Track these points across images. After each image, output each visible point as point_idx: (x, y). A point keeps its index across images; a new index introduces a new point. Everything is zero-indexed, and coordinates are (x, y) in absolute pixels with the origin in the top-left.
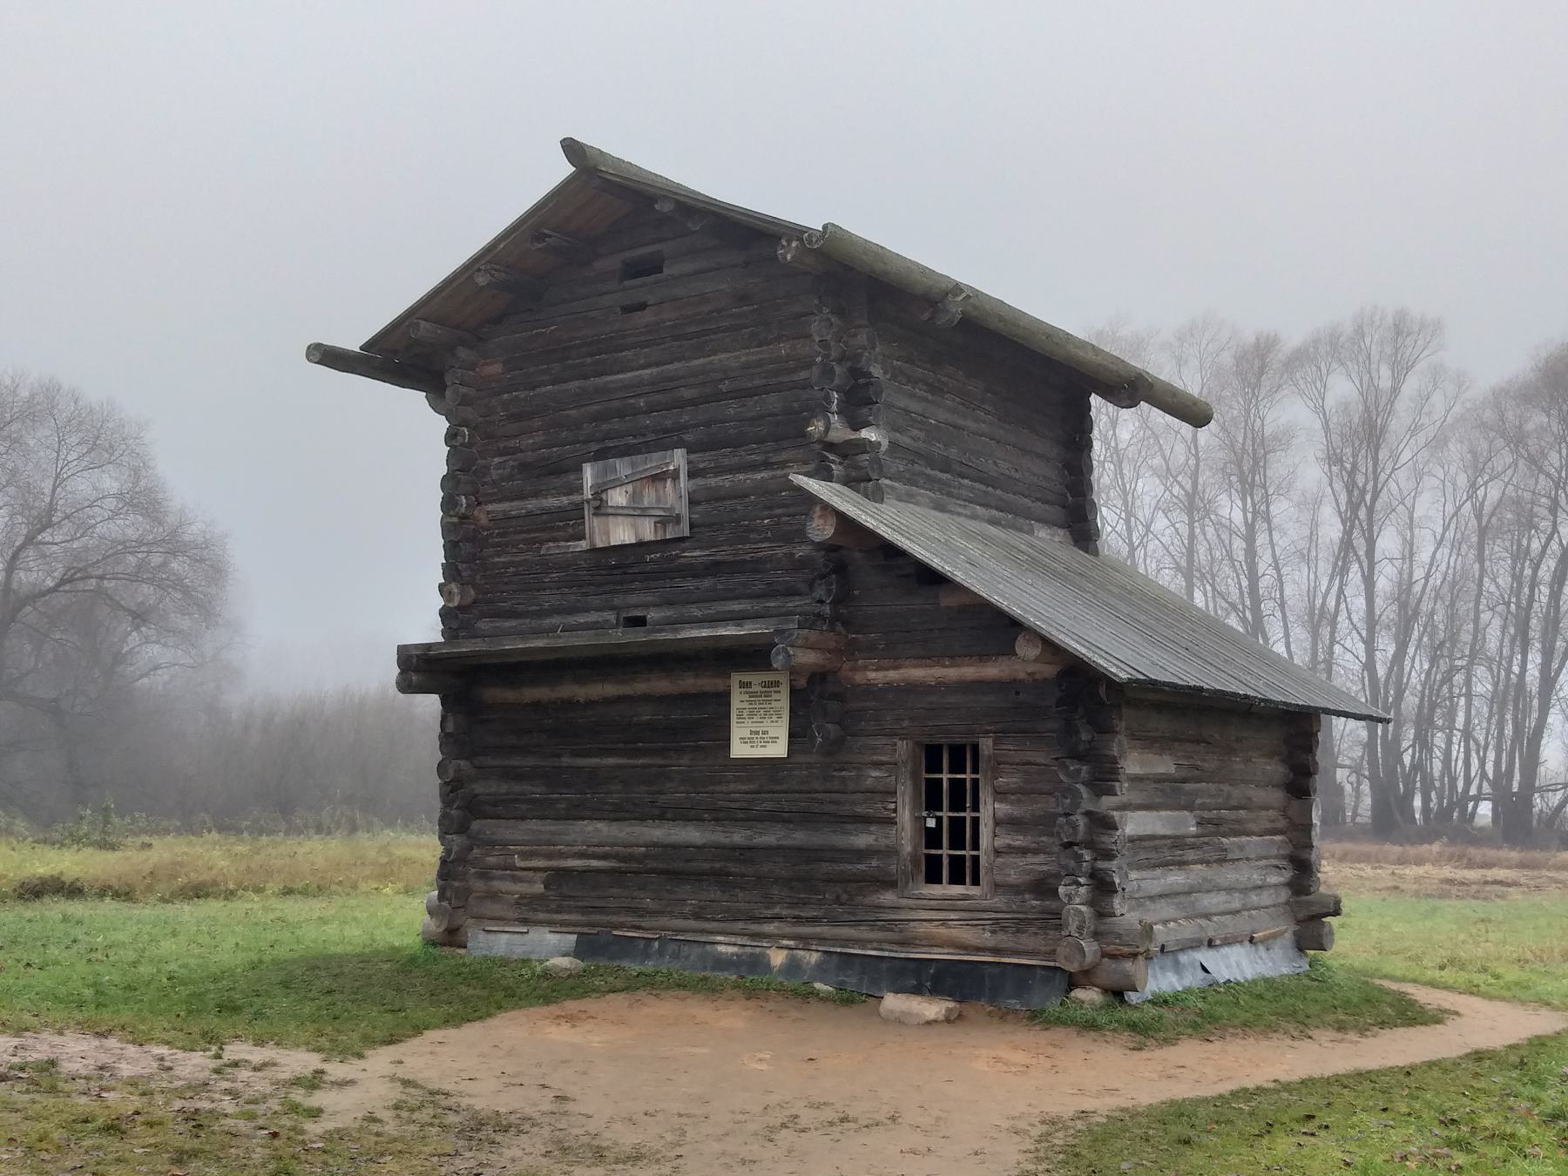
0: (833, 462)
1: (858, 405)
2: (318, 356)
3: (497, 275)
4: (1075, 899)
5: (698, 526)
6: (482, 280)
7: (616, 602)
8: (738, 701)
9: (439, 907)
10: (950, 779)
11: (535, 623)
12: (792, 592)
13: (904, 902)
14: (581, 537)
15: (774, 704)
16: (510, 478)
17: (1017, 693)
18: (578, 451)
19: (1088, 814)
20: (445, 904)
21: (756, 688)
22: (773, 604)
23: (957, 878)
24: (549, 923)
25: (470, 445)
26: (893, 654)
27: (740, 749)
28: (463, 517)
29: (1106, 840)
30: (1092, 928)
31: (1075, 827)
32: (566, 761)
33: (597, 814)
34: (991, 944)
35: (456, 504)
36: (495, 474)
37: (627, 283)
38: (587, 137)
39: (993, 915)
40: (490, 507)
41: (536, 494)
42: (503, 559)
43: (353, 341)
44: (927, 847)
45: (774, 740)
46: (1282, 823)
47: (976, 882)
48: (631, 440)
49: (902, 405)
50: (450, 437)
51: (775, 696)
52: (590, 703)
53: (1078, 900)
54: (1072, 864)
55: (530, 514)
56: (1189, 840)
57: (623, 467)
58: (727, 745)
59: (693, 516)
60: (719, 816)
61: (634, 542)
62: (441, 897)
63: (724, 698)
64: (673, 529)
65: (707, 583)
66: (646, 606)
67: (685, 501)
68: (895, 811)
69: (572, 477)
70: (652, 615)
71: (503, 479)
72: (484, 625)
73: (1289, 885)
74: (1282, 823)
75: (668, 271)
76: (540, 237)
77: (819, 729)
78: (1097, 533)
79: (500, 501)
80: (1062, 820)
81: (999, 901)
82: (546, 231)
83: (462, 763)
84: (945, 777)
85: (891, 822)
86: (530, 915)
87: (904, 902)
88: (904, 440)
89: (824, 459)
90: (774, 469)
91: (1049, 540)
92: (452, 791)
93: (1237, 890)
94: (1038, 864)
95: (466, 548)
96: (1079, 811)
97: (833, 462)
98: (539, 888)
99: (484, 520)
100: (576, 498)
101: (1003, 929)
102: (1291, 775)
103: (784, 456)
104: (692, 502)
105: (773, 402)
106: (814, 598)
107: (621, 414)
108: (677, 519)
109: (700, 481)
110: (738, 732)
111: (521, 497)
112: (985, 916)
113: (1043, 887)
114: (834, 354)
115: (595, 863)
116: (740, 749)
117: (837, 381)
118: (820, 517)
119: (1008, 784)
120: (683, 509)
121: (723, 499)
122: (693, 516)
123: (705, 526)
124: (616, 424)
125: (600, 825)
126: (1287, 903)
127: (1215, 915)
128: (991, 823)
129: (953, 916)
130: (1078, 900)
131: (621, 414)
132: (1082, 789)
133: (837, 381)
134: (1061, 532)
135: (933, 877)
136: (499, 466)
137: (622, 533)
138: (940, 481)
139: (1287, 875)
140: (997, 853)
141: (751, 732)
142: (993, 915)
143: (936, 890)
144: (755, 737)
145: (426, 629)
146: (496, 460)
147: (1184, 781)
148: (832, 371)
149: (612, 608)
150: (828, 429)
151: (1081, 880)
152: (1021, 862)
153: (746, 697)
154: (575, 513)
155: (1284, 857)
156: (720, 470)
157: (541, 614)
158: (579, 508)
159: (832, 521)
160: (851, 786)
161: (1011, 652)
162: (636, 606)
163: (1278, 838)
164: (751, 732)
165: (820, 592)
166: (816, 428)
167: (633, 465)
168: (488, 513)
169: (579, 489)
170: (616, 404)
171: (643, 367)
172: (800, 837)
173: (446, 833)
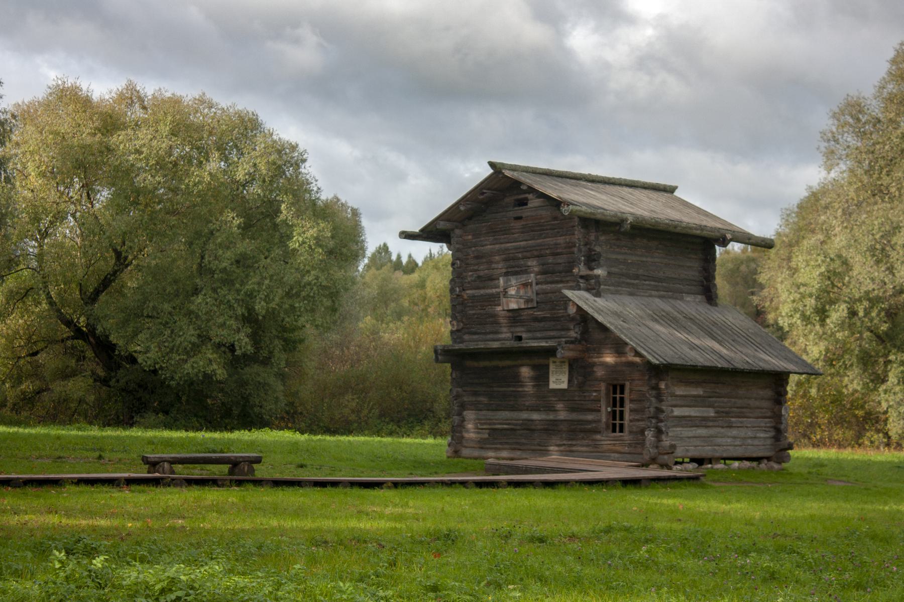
1: (592, 260)
2: (403, 236)
6: (462, 208)
8: (552, 368)
13: (603, 438)
19: (656, 408)
24: (491, 449)
25: (460, 267)
27: (552, 386)
28: (458, 296)
29: (662, 416)
32: (495, 389)
33: (506, 408)
35: (455, 291)
36: (469, 279)
37: (516, 208)
38: (497, 160)
40: (468, 292)
41: (484, 288)
43: (417, 229)
45: (563, 382)
46: (769, 414)
48: (517, 269)
52: (503, 368)
54: (649, 424)
55: (482, 295)
57: (513, 281)
58: (548, 385)
63: (547, 366)
65: (542, 324)
66: (522, 332)
67: (535, 294)
69: (497, 282)
71: (472, 281)
72: (466, 337)
73: (774, 437)
74: (769, 414)
75: (530, 205)
77: (576, 378)
78: (717, 297)
79: (471, 289)
82: (485, 191)
83: (459, 389)
85: (599, 411)
86: (483, 446)
87: (603, 438)
88: (614, 270)
89: (578, 282)
91: (692, 305)
93: (738, 438)
95: (459, 308)
98: (486, 436)
99: (465, 297)
100: (497, 290)
101: (631, 446)
103: (568, 279)
108: (532, 300)
109: (540, 286)
110: (552, 379)
111: (478, 288)
114: (582, 243)
115: (505, 426)
116: (552, 386)
117: (583, 253)
120: (534, 297)
121: (548, 293)
123: (542, 303)
125: (507, 413)
126: (772, 445)
134: (699, 297)
135: (614, 431)
136: (472, 276)
138: (633, 284)
139: (772, 434)
140: (631, 421)
143: (614, 434)
144: (558, 381)
145: (445, 339)
146: (470, 273)
147: (710, 397)
155: (771, 427)
156: (547, 283)
157: (486, 333)
158: (498, 294)
159: (575, 307)
160: (587, 399)
163: (767, 420)
166: (575, 271)
167: (517, 279)
170: (511, 255)
171: (521, 241)
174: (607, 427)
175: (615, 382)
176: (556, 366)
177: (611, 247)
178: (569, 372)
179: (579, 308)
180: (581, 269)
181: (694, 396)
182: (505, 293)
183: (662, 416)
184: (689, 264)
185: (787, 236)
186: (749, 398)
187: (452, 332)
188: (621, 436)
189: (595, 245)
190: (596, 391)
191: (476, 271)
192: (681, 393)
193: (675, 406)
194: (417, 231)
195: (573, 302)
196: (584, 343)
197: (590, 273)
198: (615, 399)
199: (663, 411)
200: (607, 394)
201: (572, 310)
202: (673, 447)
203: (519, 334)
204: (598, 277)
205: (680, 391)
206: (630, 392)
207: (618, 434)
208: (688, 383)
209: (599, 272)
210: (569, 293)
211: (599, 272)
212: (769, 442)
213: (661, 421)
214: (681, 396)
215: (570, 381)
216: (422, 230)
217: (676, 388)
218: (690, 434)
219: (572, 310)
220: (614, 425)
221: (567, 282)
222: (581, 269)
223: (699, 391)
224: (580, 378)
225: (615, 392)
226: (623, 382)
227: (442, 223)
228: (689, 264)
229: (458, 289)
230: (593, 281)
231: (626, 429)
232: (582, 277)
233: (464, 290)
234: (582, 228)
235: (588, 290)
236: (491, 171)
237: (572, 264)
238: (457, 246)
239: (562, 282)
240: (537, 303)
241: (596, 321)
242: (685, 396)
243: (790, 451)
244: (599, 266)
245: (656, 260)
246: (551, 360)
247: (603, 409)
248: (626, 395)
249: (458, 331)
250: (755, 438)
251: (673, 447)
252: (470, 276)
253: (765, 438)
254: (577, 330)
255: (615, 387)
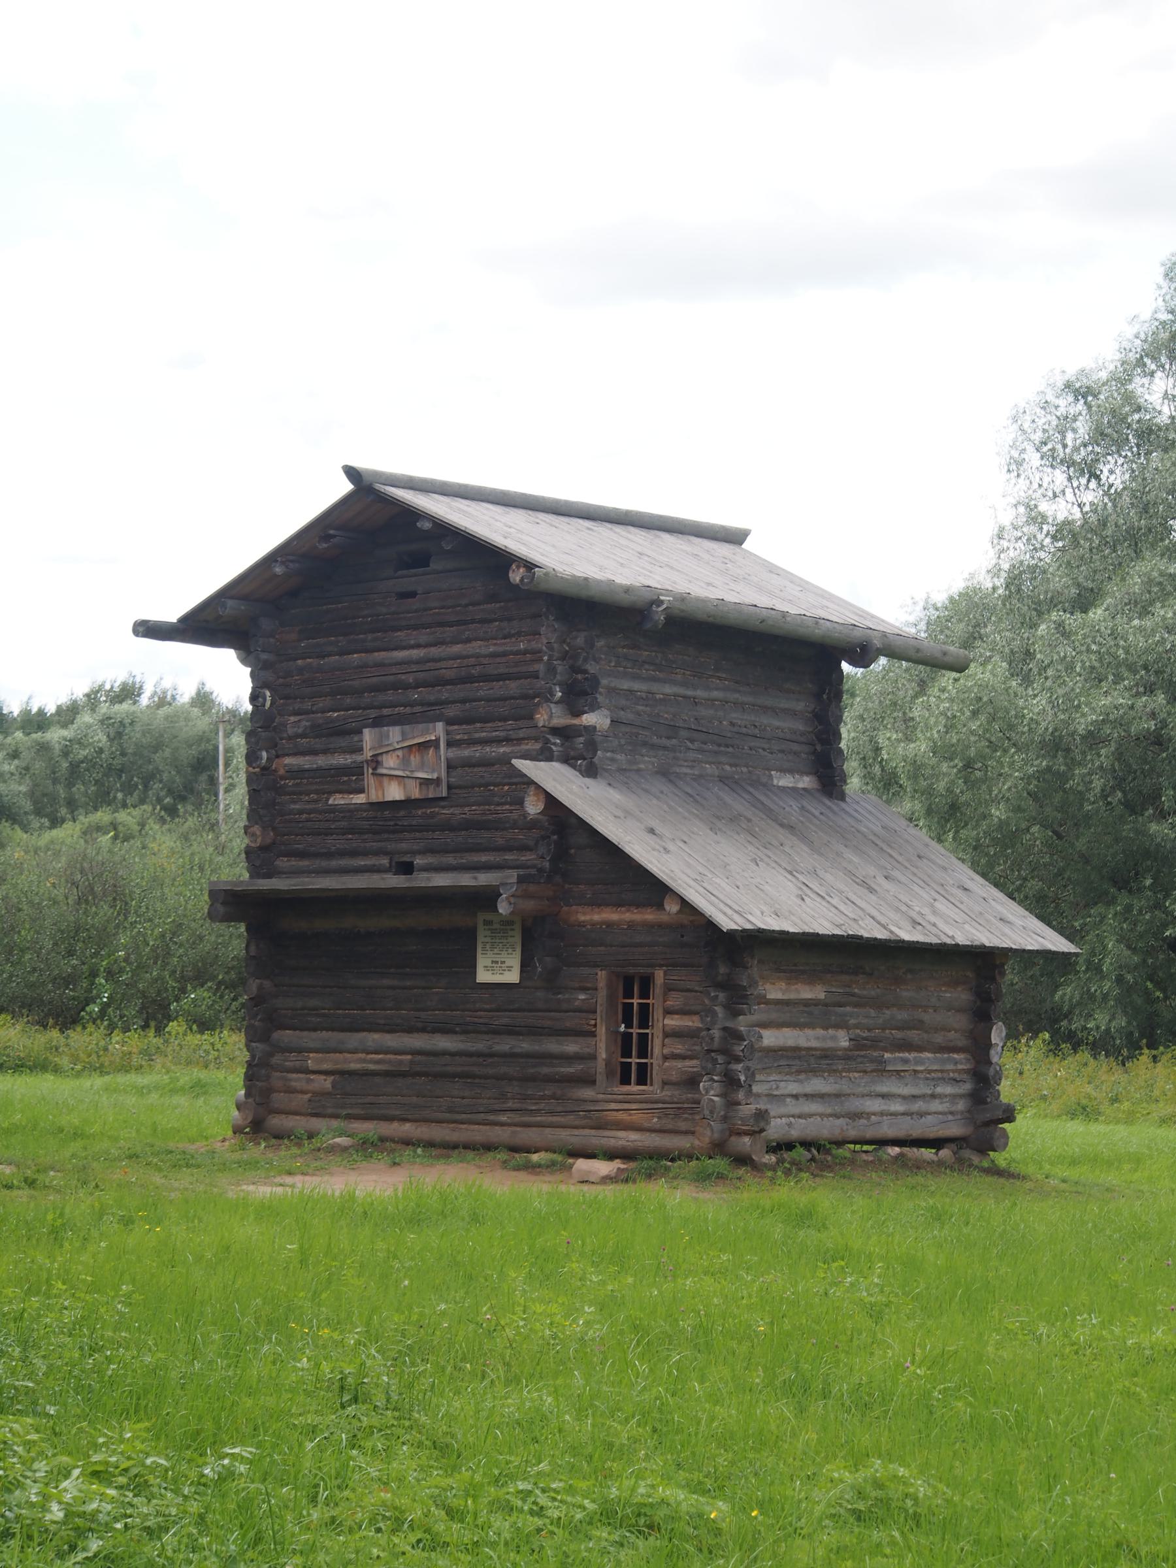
0: (555, 744)
3: (291, 565)
4: (711, 1092)
5: (456, 788)
6: (278, 570)
7: (390, 846)
8: (482, 936)
9: (246, 1103)
10: (639, 1004)
11: (324, 863)
12: (524, 848)
14: (362, 791)
15: (510, 940)
16: (303, 736)
17: (682, 936)
18: (359, 716)
19: (725, 1029)
20: (250, 1100)
21: (496, 926)
22: (512, 857)
23: (642, 1081)
26: (597, 903)
27: (484, 976)
28: (264, 769)
29: (738, 1049)
30: (722, 1113)
31: (712, 1039)
34: (658, 1126)
35: (260, 758)
36: (291, 731)
37: (400, 573)
38: (362, 463)
39: (661, 1106)
40: (288, 760)
42: (297, 807)
43: (172, 614)
44: (622, 1057)
45: (510, 968)
47: (651, 1085)
49: (625, 687)
50: (252, 675)
51: (511, 933)
53: (712, 1092)
54: (710, 1066)
56: (840, 1053)
57: (394, 734)
58: (471, 966)
59: (451, 779)
60: (466, 1030)
61: (403, 798)
62: (247, 1095)
64: (435, 789)
68: (595, 1025)
69: (356, 739)
70: (418, 861)
72: (283, 863)
74: (962, 1042)
75: (433, 566)
76: (327, 538)
79: (295, 754)
80: (704, 1033)
81: (667, 1093)
82: (332, 532)
84: (635, 1001)
85: (593, 1034)
88: (625, 716)
89: (547, 741)
90: (514, 745)
92: (256, 1006)
94: (692, 1066)
96: (717, 1026)
97: (555, 744)
100: (359, 758)
102: (978, 1003)
104: (450, 766)
105: (513, 687)
106: (538, 855)
107: (395, 687)
110: (482, 961)
112: (656, 1106)
113: (692, 1082)
114: (556, 654)
116: (484, 976)
118: (534, 795)
119: (673, 1006)
122: (451, 779)
124: (390, 696)
127: (874, 1114)
128: (661, 1035)
129: (634, 1106)
130: (712, 1092)
131: (395, 687)
132: (718, 1009)
133: (558, 677)
135: (626, 1080)
137: (394, 792)
139: (967, 1087)
140: (666, 1058)
141: (493, 962)
142: (661, 1106)
143: (626, 1088)
146: (293, 719)
148: (554, 669)
149: (386, 853)
150: (551, 717)
151: (715, 1078)
152: (679, 1064)
153: (488, 933)
154: (357, 771)
157: (329, 855)
159: (542, 797)
161: (660, 906)
162: (406, 853)
164: (493, 962)
165: (542, 850)
168: (286, 765)
169: (360, 750)
172: (525, 1045)
173: (251, 1041)
174: (610, 1074)
175: (631, 970)
176: (493, 931)
177: (618, 665)
178: (523, 945)
179: (552, 802)
180: (551, 715)
181: (807, 1003)
182: (376, 762)
183: (738, 1049)
184: (784, 704)
185: (1127, 652)
186: (925, 1008)
187: (249, 852)
188: (643, 1093)
189: (586, 660)
190: (584, 989)
191: (306, 712)
192: (779, 996)
193: (765, 1025)
194: (175, 621)
195: (538, 787)
196: (558, 879)
197: (576, 721)
198: (628, 1008)
199: (740, 1037)
200: (611, 998)
201: (533, 807)
202: (761, 1115)
203: (407, 859)
204: (590, 730)
205: (775, 991)
206: (665, 994)
207: (634, 1088)
208: (794, 975)
209: (589, 719)
210: (525, 766)
211: (589, 719)
212: (961, 1106)
213: (738, 1060)
214: (778, 1002)
215: (525, 965)
216: (185, 619)
217: (768, 986)
218: (793, 1088)
219: (533, 807)
220: (626, 1067)
221: (520, 740)
222: (551, 715)
223: (816, 992)
224: (548, 959)
225: (629, 994)
226: (649, 970)
227: (230, 603)
228: (784, 704)
229: (264, 754)
230: (582, 739)
231: (656, 1074)
232: (556, 731)
233: (277, 756)
234: (556, 619)
235: (567, 760)
236: (346, 487)
237: (528, 702)
238: (264, 656)
239: (508, 740)
240: (449, 787)
241: (594, 833)
242: (787, 1003)
243: (1006, 1126)
244: (594, 707)
245: (716, 694)
246: (482, 917)
247: (602, 1031)
248: (656, 1002)
249: (263, 848)
250: (933, 1096)
251: (761, 1115)
252: (294, 724)
253: (954, 1097)
254: (542, 850)
255: (628, 982)
